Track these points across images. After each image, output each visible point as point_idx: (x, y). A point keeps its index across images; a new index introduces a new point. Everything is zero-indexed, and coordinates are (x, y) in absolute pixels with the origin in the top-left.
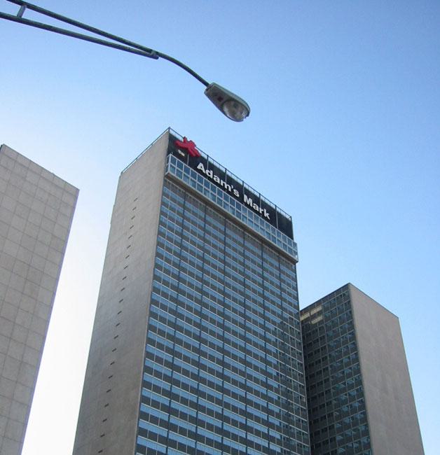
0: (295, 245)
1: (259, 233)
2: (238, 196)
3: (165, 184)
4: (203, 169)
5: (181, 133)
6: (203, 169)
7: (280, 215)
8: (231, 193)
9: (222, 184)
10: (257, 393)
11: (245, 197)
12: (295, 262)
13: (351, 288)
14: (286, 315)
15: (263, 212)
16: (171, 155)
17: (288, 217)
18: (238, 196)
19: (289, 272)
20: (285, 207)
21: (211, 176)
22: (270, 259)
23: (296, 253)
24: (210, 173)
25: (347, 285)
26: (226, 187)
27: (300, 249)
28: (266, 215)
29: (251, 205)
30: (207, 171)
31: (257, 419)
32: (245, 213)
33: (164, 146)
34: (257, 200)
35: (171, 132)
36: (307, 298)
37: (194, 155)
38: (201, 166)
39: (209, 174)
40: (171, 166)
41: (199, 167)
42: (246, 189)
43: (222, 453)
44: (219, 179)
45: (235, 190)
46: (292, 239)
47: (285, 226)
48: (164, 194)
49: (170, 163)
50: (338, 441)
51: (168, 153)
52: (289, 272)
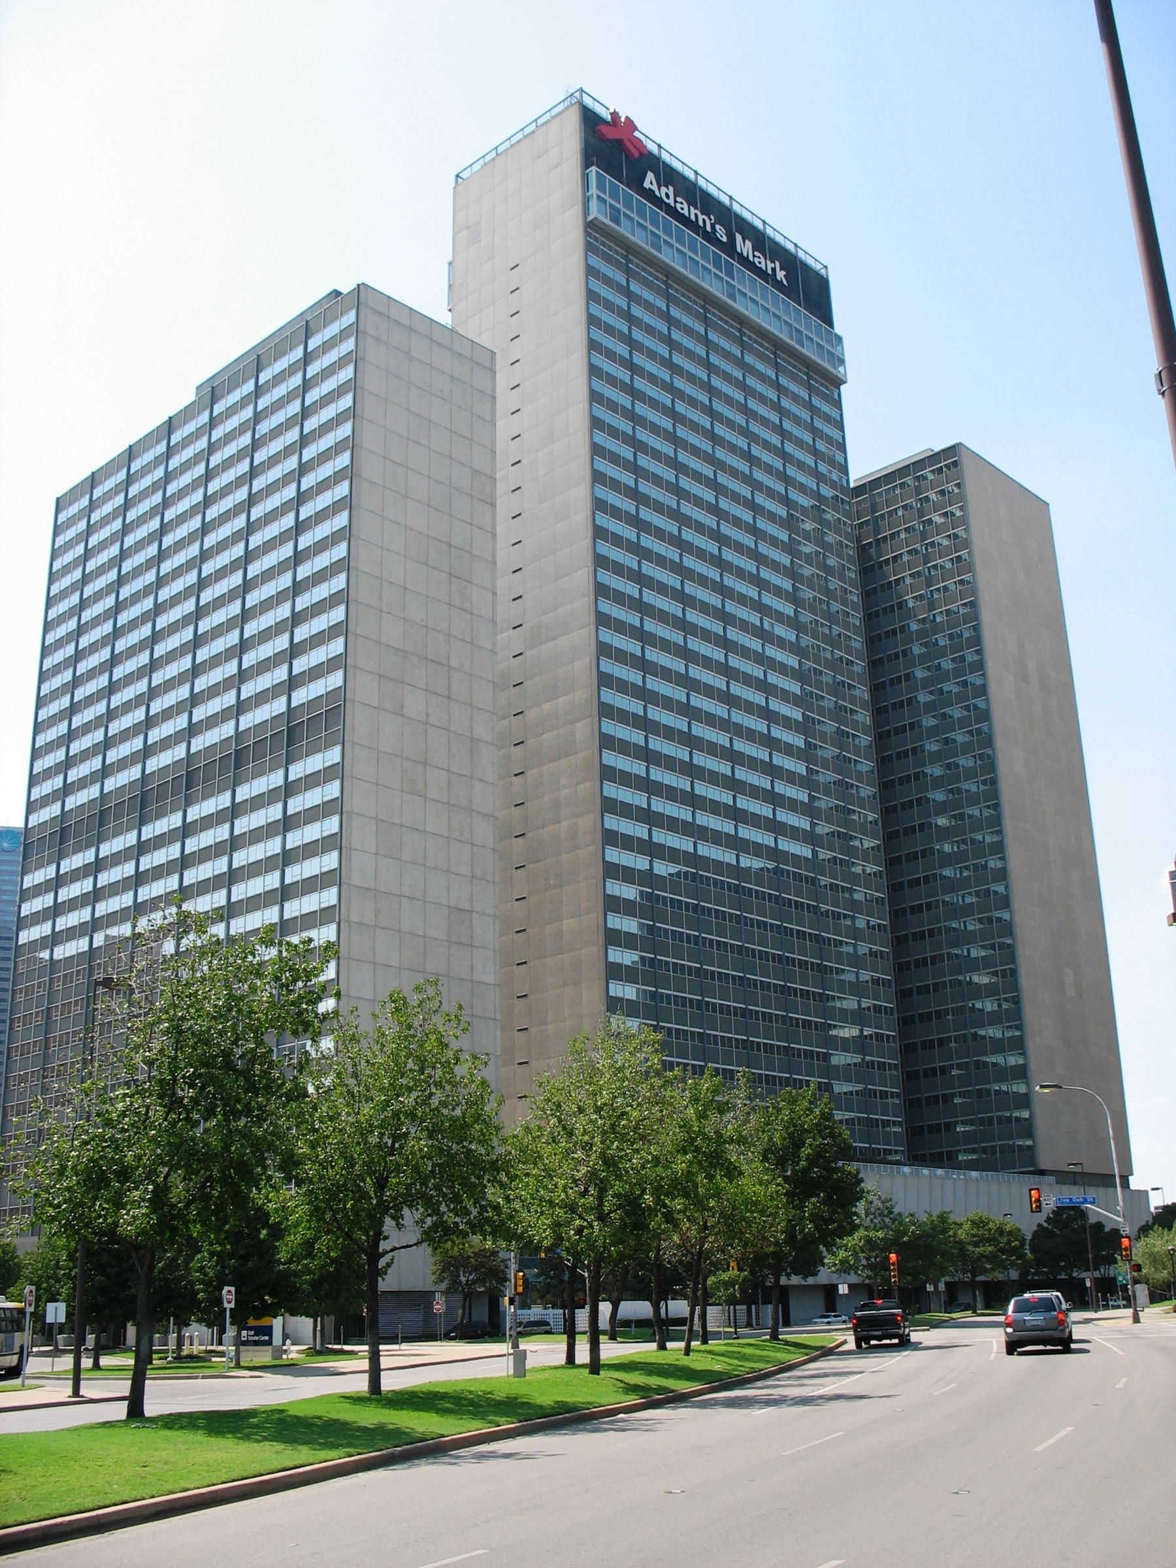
0: (839, 339)
1: (773, 327)
2: (725, 239)
3: (590, 248)
4: (655, 187)
5: (610, 100)
6: (655, 187)
7: (805, 267)
8: (710, 237)
9: (693, 218)
10: (653, 379)
11: (739, 238)
12: (837, 382)
13: (967, 465)
14: (827, 491)
15: (774, 270)
16: (594, 168)
17: (818, 267)
18: (725, 239)
19: (825, 408)
20: (812, 243)
21: (671, 202)
22: (794, 387)
23: (842, 362)
24: (666, 193)
25: (953, 447)
26: (701, 223)
27: (850, 351)
28: (781, 275)
29: (751, 258)
30: (664, 190)
31: (698, 502)
32: (744, 281)
33: (569, 141)
34: (761, 241)
35: (588, 101)
36: (864, 463)
37: (637, 155)
38: (650, 181)
39: (667, 196)
40: (598, 197)
41: (647, 185)
42: (739, 218)
43: (861, 1031)
44: (685, 206)
45: (718, 227)
46: (831, 325)
47: (809, 289)
48: (590, 271)
49: (594, 190)
50: (927, 728)
51: (587, 164)
52: (825, 408)
